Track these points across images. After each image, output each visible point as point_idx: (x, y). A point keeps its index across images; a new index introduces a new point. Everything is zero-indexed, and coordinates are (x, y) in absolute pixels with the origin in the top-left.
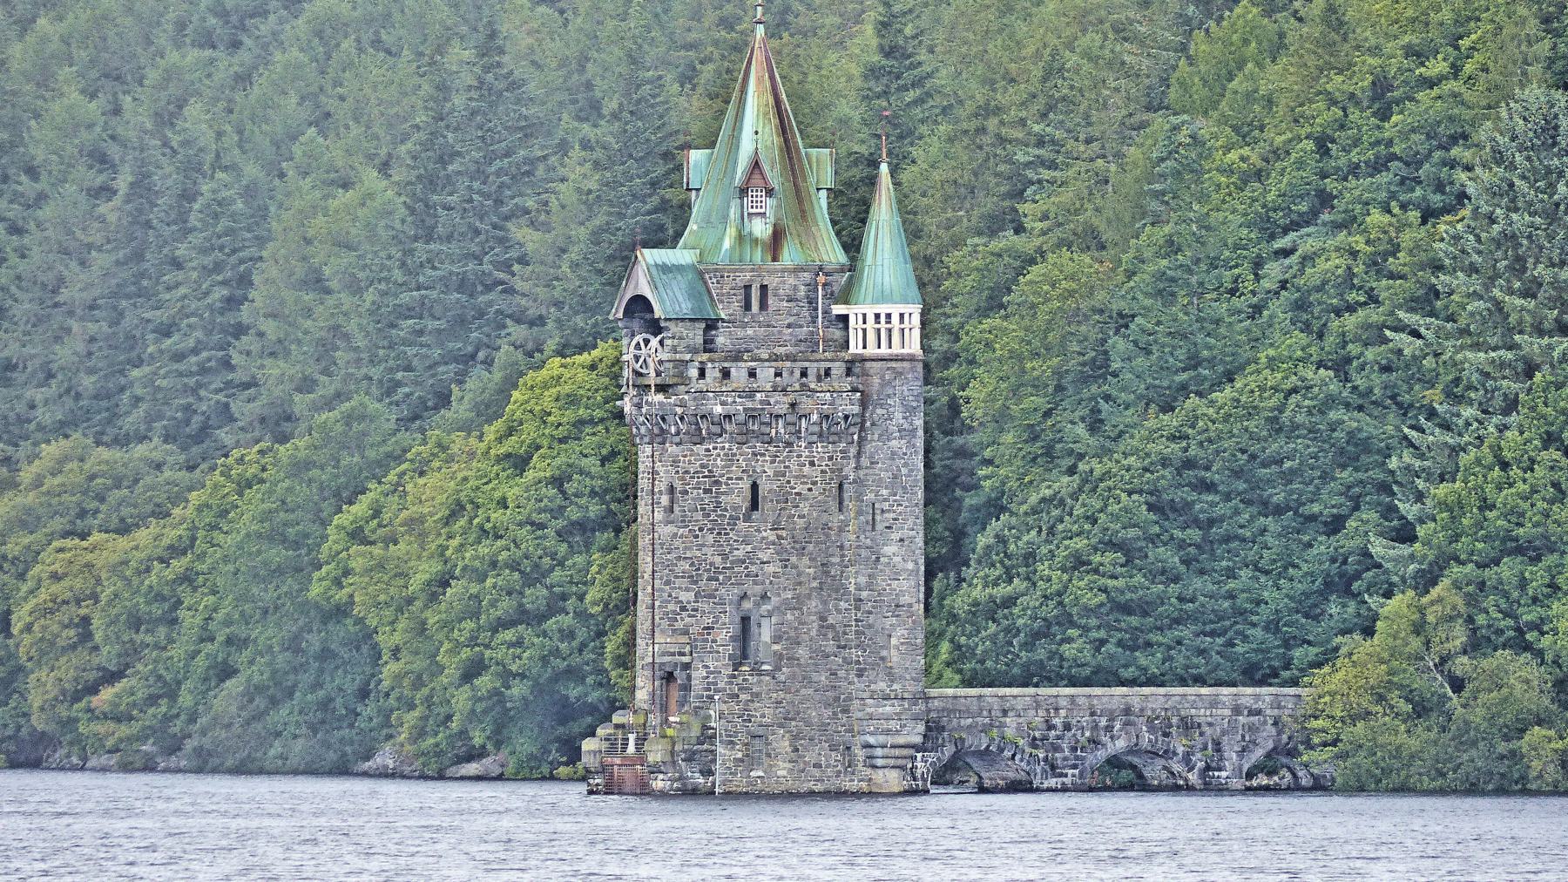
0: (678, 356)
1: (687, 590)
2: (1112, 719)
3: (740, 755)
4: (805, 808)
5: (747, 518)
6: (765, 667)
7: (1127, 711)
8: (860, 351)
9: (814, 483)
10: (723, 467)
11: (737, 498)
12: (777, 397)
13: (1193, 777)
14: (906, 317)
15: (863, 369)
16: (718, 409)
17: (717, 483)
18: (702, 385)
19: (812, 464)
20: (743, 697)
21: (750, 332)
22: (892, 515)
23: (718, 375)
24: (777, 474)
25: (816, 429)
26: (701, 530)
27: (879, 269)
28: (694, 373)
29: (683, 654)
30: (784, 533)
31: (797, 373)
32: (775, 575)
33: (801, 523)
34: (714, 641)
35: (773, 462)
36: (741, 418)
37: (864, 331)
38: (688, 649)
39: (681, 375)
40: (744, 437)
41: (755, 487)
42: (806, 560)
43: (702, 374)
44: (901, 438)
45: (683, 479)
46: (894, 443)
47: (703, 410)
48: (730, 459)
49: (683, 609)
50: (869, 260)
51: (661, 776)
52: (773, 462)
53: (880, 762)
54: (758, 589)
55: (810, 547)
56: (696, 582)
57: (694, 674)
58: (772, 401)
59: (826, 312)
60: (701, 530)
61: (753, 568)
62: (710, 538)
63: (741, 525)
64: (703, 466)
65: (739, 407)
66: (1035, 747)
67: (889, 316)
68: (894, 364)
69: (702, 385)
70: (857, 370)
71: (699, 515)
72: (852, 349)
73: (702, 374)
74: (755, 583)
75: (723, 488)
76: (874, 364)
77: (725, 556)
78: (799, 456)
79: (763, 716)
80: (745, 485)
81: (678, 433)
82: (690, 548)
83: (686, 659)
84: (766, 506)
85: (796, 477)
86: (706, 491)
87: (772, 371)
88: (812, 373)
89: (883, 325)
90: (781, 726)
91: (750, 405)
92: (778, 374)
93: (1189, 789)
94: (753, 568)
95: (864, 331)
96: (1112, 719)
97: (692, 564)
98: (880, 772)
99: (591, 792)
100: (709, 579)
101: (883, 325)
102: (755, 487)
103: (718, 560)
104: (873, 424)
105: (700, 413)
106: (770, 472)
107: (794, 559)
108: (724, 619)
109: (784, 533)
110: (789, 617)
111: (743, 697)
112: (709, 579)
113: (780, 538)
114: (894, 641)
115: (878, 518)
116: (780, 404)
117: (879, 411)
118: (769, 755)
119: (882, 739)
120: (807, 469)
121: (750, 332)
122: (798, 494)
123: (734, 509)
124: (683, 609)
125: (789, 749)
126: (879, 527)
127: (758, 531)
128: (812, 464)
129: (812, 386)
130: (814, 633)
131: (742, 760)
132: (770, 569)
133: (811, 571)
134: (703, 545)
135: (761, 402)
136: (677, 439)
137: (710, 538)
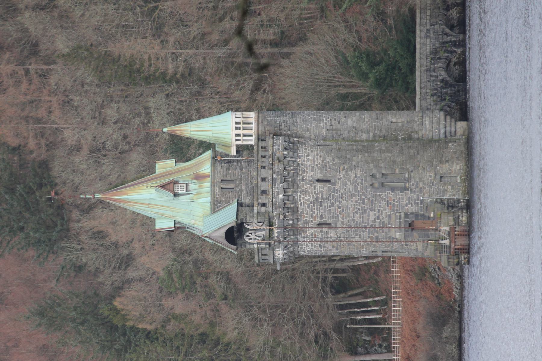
0: (255, 215)
1: (369, 215)
2: (431, 76)
3: (450, 187)
4: (466, 307)
5: (334, 184)
6: (407, 176)
7: (429, 70)
8: (253, 138)
9: (317, 155)
10: (309, 196)
11: (324, 188)
12: (276, 168)
13: (459, 50)
14: (237, 126)
15: (262, 135)
16: (281, 196)
17: (317, 199)
18: (269, 205)
19: (308, 156)
20: (421, 185)
21: (244, 188)
22: (333, 121)
23: (264, 196)
24: (313, 171)
25: (291, 153)
26: (340, 208)
27: (214, 128)
28: (263, 209)
29: (400, 216)
30: (342, 167)
31: (263, 159)
32: (362, 171)
33: (336, 160)
34: (394, 200)
35: (307, 172)
36: (285, 185)
37: (244, 135)
38: (398, 214)
39: (264, 214)
40: (294, 184)
41: (318, 181)
42: (355, 158)
43: (264, 205)
44: (296, 117)
45: (315, 218)
46: (298, 120)
47: (281, 204)
48: (305, 192)
49: (378, 218)
50: (209, 134)
51: (461, 218)
52: (307, 172)
53: (453, 129)
54: (369, 179)
55: (348, 156)
56: (365, 210)
57: (410, 211)
58: (277, 170)
59: (235, 157)
60: (340, 208)
61: (359, 181)
62: (344, 202)
63: (337, 186)
64: (309, 207)
65: (280, 186)
66: (445, 99)
67: (237, 123)
68: (260, 120)
69: (269, 205)
70: (263, 138)
71: (333, 208)
72: (252, 143)
73: (264, 205)
74: (366, 180)
75: (320, 196)
76: (260, 129)
77: (353, 195)
78: (304, 161)
79: (431, 176)
80: (318, 185)
81: (293, 220)
82: (349, 214)
83: (403, 215)
84: (328, 175)
85: (314, 162)
86: (321, 205)
87: (262, 170)
88: (263, 154)
89: (241, 126)
90: (436, 168)
91: (279, 181)
92: (264, 168)
93: (464, 53)
94: (359, 181)
95: (244, 135)
96: (431, 76)
97: (357, 212)
98: (458, 130)
99: (469, 262)
100: (364, 203)
101: (241, 126)
102: (318, 181)
103: (354, 199)
104: (289, 130)
105: (282, 206)
106: (312, 173)
107: (354, 163)
108: (383, 195)
109: (342, 167)
110: (382, 165)
111: (421, 185)
112: (364, 203)
113: (343, 169)
114: (394, 120)
115: (334, 127)
116: (278, 167)
117: (283, 127)
118: (450, 173)
119: (442, 126)
120: (310, 158)
121: (244, 188)
122: (323, 161)
123: (329, 190)
124: (378, 218)
125: (447, 164)
126: (339, 126)
127: (341, 178)
128: (308, 156)
129: (270, 153)
130: (390, 155)
131: (452, 186)
132: (359, 173)
133: (360, 156)
134: (347, 206)
135: (278, 175)
136: (295, 220)
137: (344, 202)
